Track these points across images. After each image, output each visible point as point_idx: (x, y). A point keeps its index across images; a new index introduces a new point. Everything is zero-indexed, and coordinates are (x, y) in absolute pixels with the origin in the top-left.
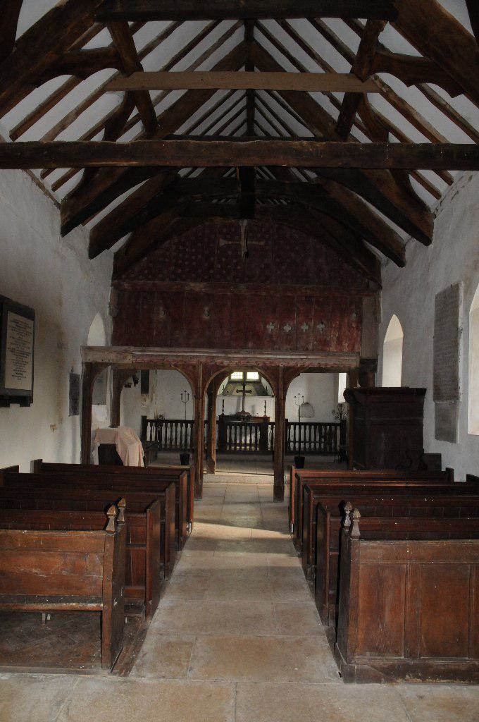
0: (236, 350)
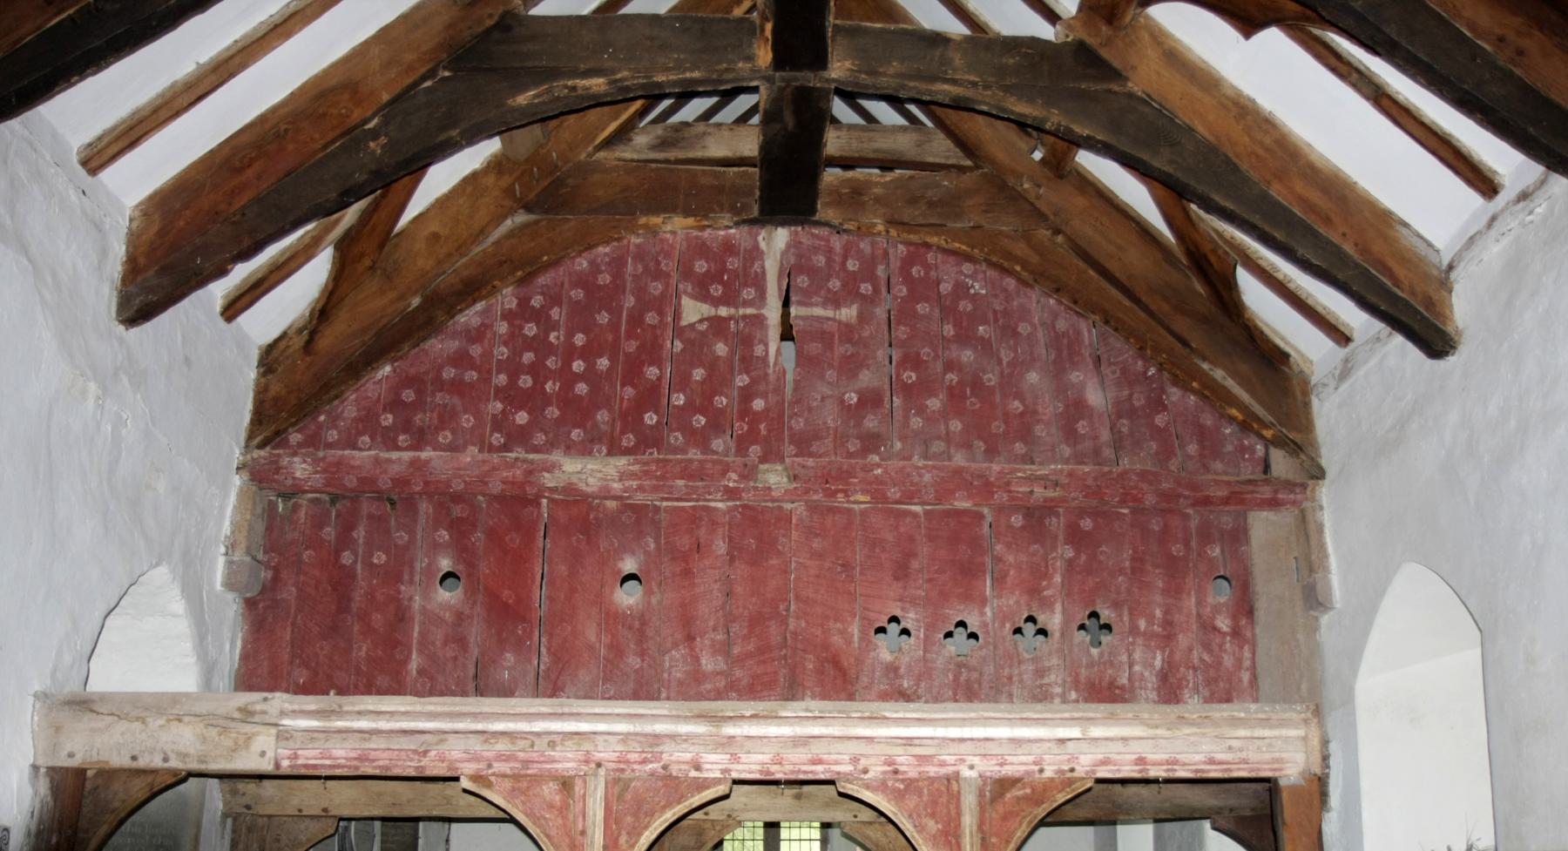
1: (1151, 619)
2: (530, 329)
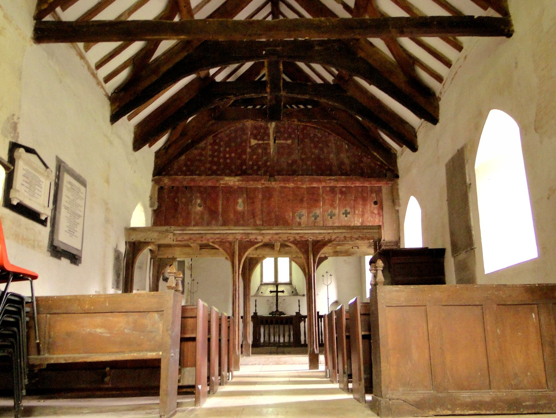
0: (269, 227)
1: (359, 211)
2: (216, 147)
